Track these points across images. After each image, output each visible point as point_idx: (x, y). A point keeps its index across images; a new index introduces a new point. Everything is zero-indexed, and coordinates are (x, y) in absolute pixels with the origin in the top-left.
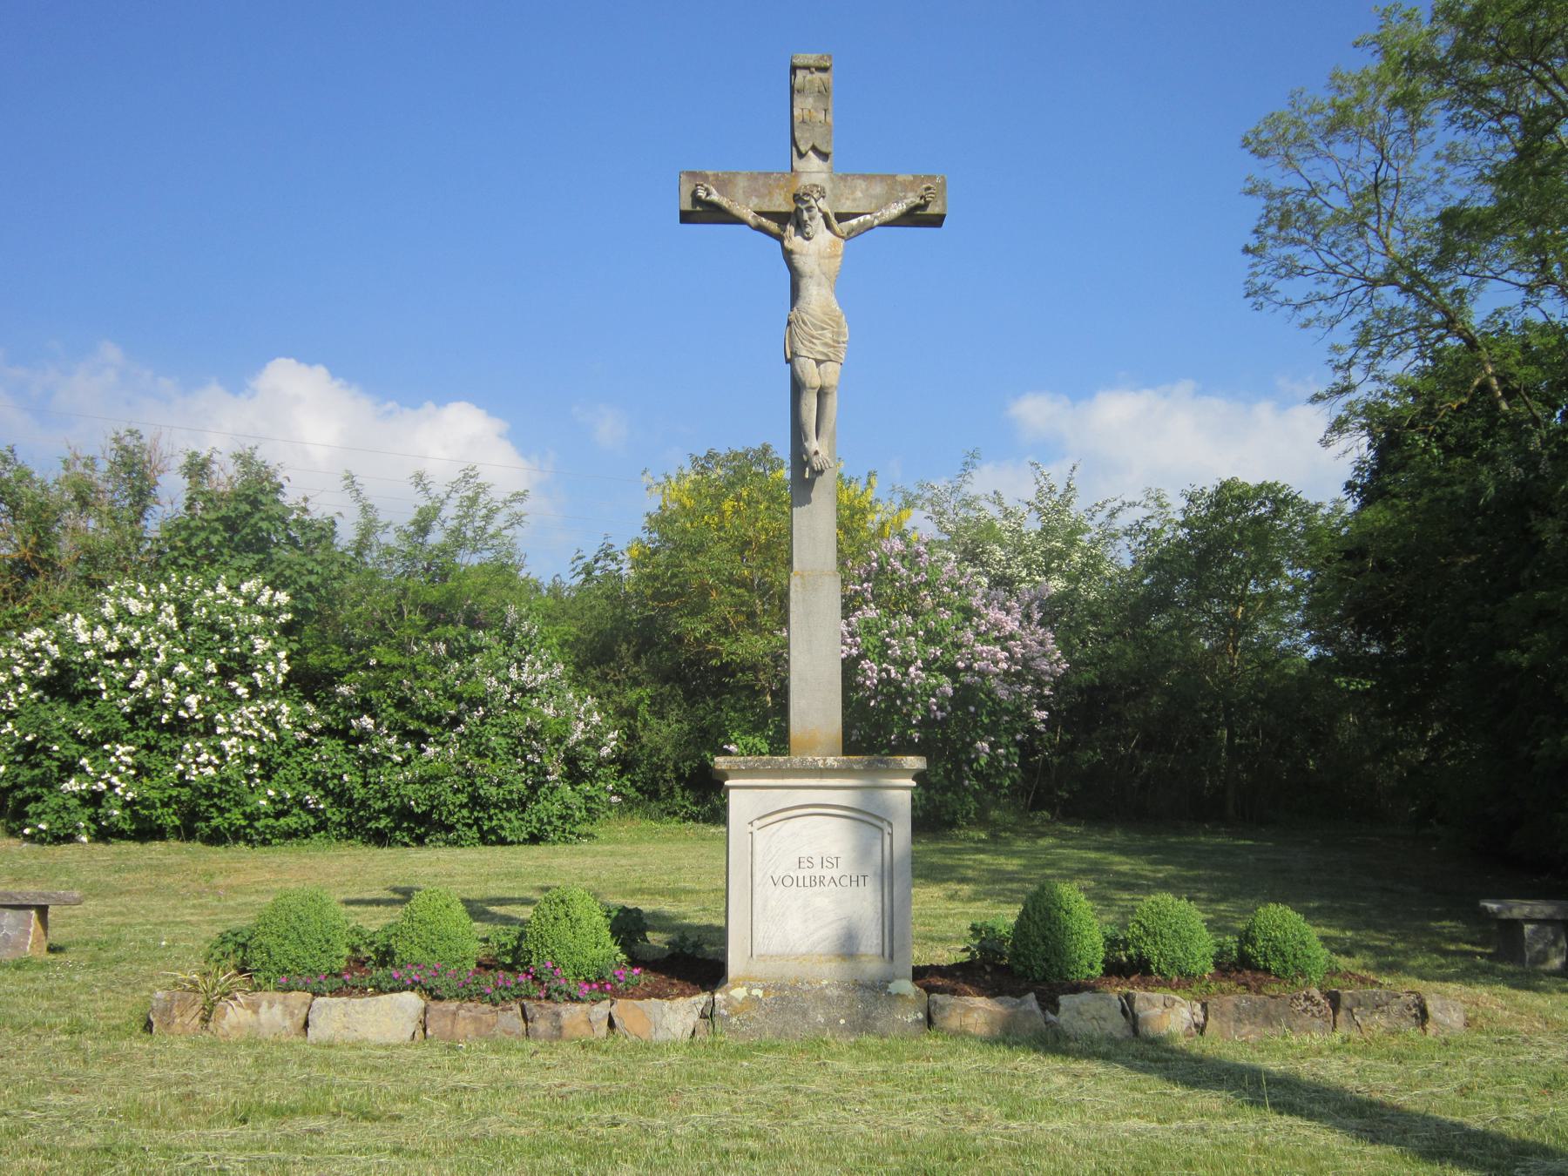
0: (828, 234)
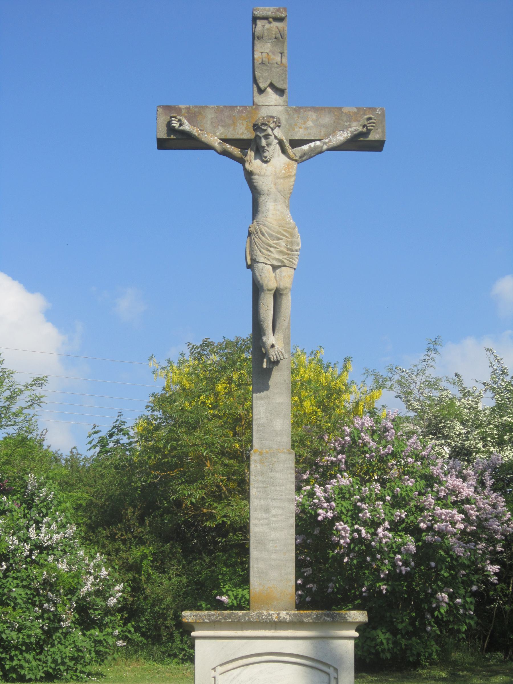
0: (283, 157)
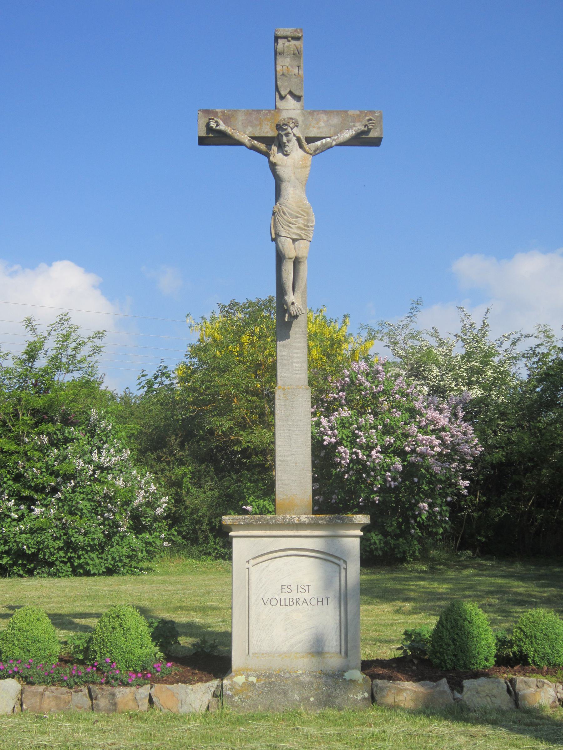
0: (300, 152)
